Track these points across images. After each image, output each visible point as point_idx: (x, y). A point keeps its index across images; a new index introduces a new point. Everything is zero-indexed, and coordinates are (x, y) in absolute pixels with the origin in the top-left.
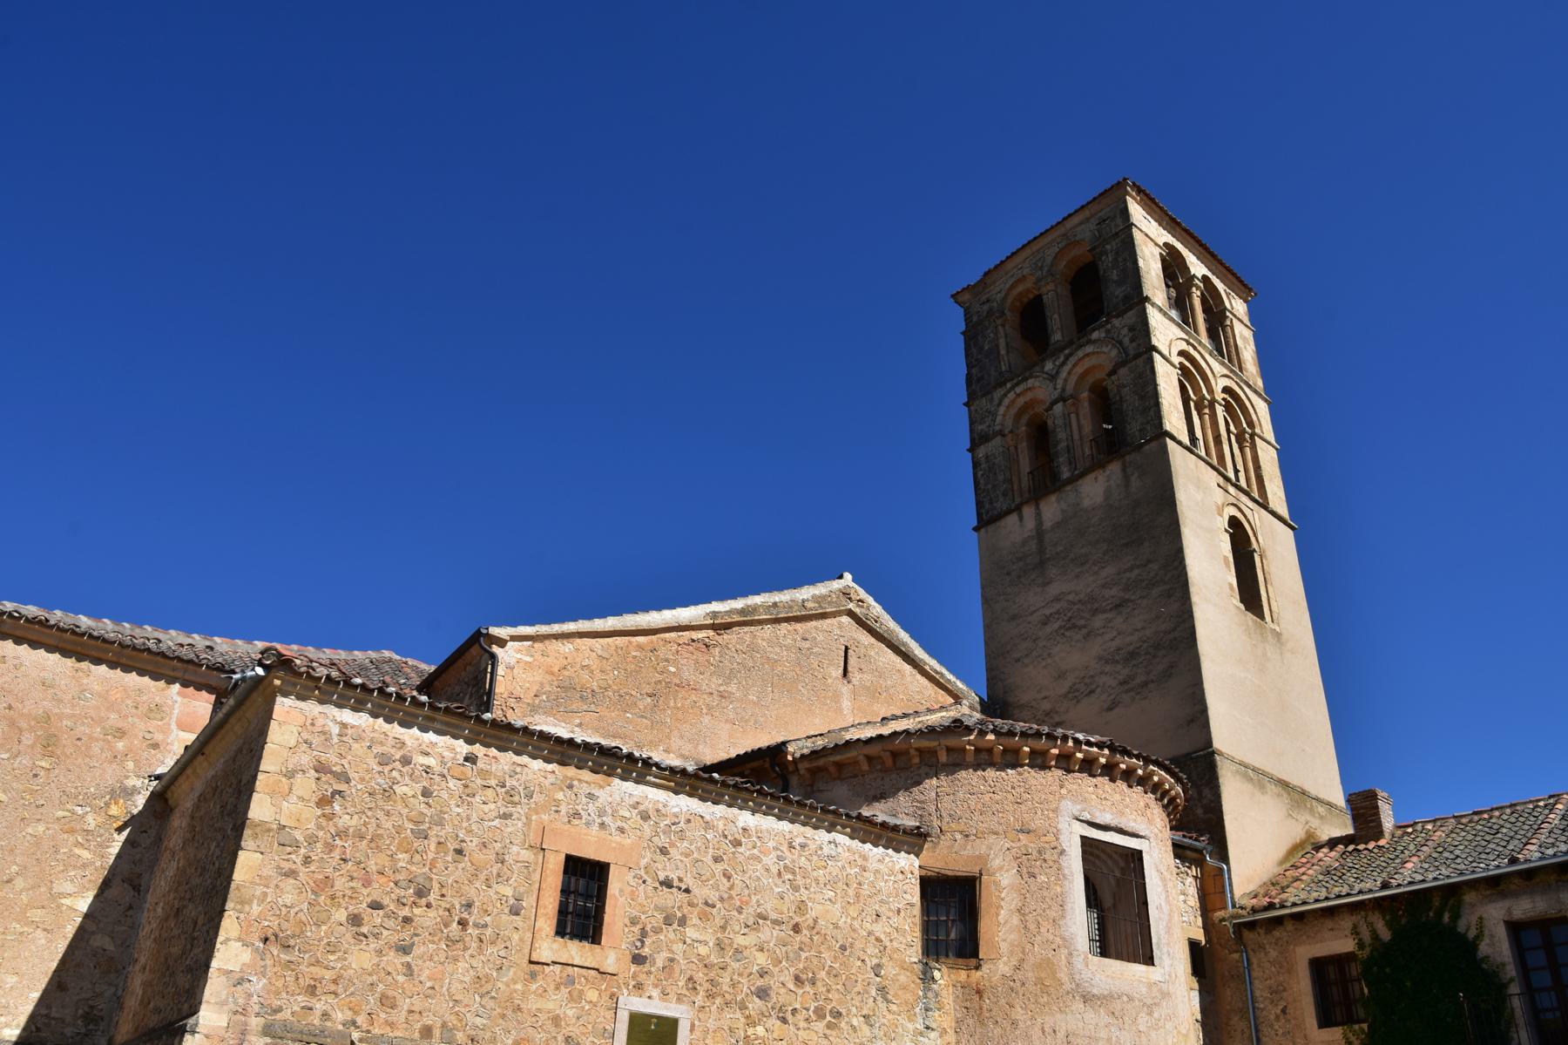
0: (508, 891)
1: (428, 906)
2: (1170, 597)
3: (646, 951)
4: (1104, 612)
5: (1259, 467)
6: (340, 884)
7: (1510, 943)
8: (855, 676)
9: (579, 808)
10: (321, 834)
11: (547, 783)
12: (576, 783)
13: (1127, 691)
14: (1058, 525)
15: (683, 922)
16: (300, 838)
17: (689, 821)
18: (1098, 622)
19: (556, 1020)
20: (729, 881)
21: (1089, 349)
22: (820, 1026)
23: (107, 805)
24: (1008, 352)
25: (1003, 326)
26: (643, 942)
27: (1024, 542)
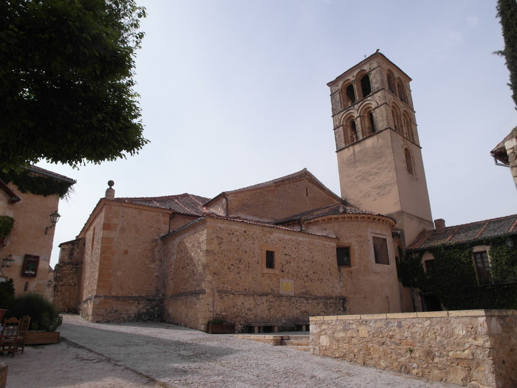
0: (256, 259)
1: (242, 264)
2: (390, 172)
3: (284, 269)
4: (372, 175)
5: (412, 132)
6: (225, 261)
8: (310, 195)
10: (220, 251)
11: (260, 235)
13: (378, 196)
15: (290, 262)
16: (216, 252)
17: (289, 240)
18: (371, 178)
19: (268, 285)
21: (367, 102)
22: (319, 282)
23: (152, 243)
24: (343, 101)
25: (342, 93)
27: (350, 156)
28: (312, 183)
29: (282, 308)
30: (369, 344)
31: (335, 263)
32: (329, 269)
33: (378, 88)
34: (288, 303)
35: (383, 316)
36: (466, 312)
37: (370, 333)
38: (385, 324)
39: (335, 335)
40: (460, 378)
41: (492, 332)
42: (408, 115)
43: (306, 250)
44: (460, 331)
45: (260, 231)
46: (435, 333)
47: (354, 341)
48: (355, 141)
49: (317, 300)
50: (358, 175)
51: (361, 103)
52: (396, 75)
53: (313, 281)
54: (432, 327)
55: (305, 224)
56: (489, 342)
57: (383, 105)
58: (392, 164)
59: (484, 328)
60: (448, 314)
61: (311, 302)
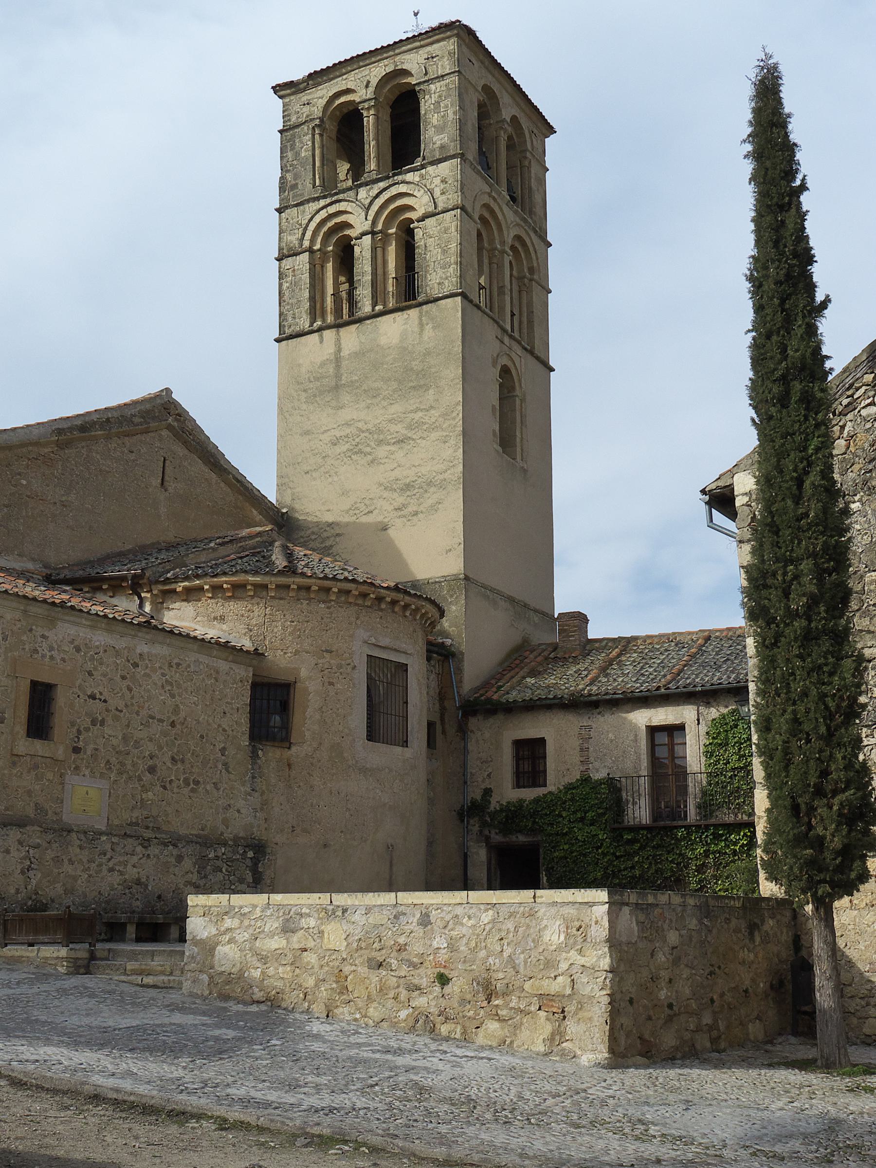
2: (445, 442)
3: (81, 744)
7: (647, 741)
8: (171, 486)
9: (37, 645)
11: (15, 628)
12: (34, 627)
14: (356, 354)
15: (102, 723)
18: (382, 452)
19: (29, 793)
20: (131, 693)
22: (186, 791)
26: (79, 738)
27: (323, 364)
28: (185, 443)
29: (67, 868)
30: (345, 966)
31: (243, 733)
32: (223, 750)
33: (442, 147)
34: (86, 852)
35: (387, 898)
36: (572, 893)
37: (350, 940)
38: (391, 917)
39: (258, 943)
40: (542, 1037)
41: (617, 936)
42: (527, 251)
43: (155, 684)
44: (554, 936)
45: (18, 615)
46: (502, 939)
47: (311, 958)
48: (346, 317)
49: (175, 846)
50: (343, 434)
51: (382, 185)
52: (508, 110)
53: (168, 786)
54: (498, 925)
55: (155, 592)
56: (608, 957)
57: (453, 213)
58: (454, 419)
59: (602, 929)
60: (534, 897)
61: (157, 851)
